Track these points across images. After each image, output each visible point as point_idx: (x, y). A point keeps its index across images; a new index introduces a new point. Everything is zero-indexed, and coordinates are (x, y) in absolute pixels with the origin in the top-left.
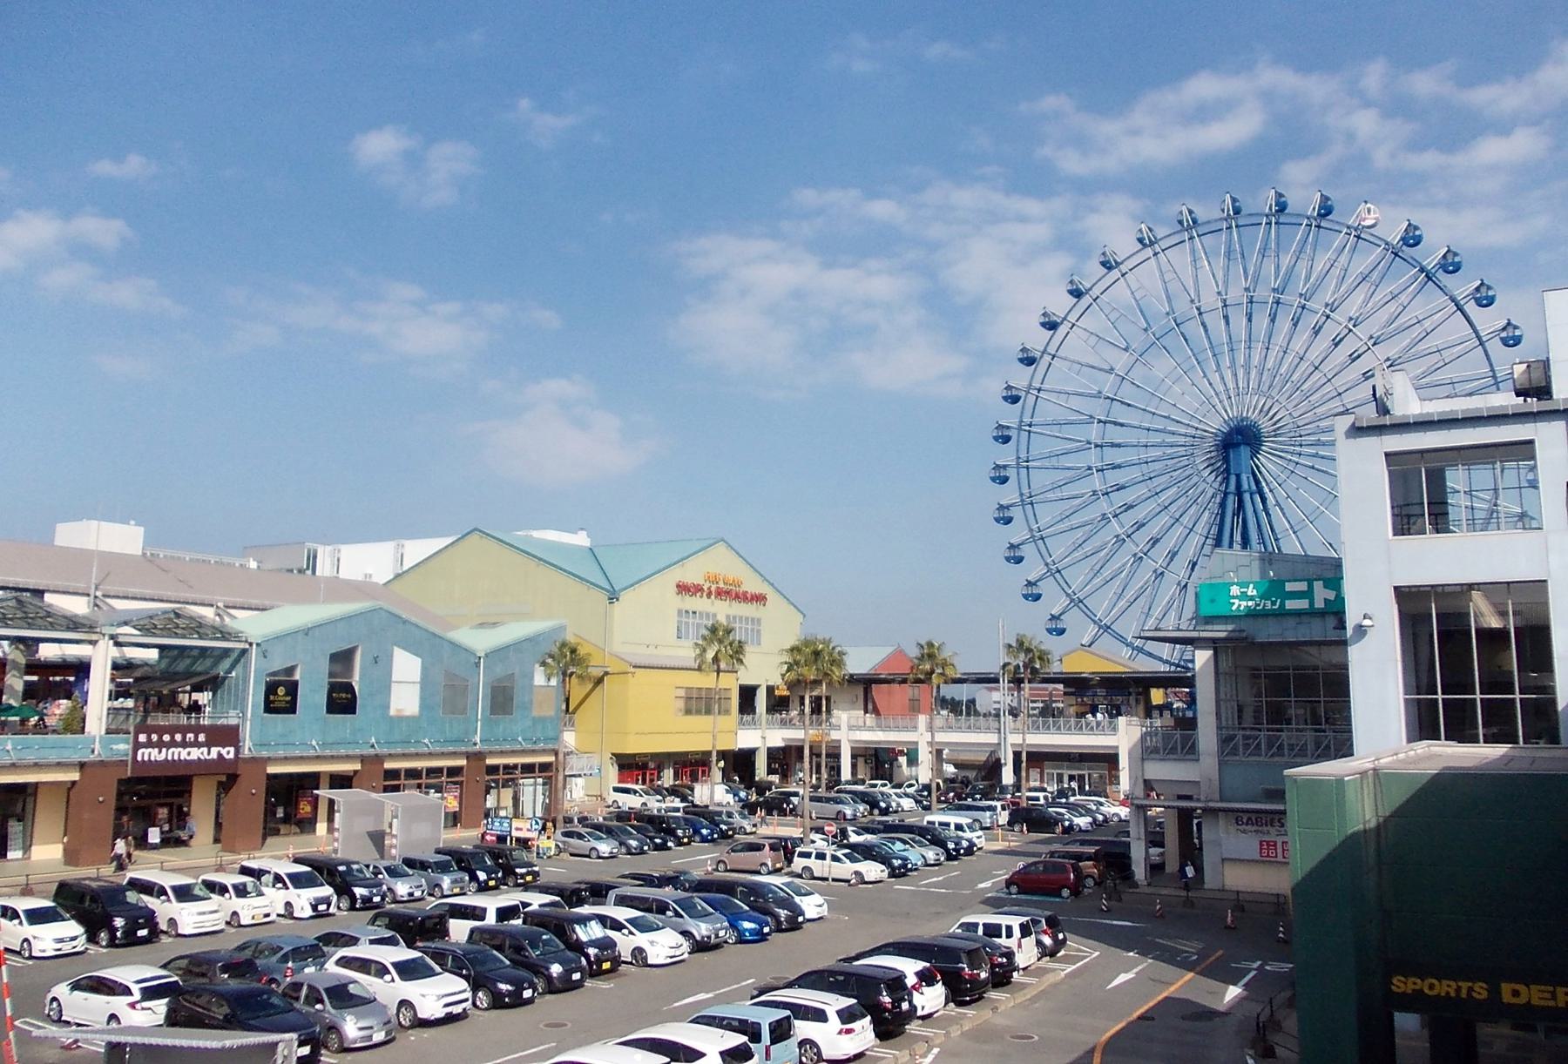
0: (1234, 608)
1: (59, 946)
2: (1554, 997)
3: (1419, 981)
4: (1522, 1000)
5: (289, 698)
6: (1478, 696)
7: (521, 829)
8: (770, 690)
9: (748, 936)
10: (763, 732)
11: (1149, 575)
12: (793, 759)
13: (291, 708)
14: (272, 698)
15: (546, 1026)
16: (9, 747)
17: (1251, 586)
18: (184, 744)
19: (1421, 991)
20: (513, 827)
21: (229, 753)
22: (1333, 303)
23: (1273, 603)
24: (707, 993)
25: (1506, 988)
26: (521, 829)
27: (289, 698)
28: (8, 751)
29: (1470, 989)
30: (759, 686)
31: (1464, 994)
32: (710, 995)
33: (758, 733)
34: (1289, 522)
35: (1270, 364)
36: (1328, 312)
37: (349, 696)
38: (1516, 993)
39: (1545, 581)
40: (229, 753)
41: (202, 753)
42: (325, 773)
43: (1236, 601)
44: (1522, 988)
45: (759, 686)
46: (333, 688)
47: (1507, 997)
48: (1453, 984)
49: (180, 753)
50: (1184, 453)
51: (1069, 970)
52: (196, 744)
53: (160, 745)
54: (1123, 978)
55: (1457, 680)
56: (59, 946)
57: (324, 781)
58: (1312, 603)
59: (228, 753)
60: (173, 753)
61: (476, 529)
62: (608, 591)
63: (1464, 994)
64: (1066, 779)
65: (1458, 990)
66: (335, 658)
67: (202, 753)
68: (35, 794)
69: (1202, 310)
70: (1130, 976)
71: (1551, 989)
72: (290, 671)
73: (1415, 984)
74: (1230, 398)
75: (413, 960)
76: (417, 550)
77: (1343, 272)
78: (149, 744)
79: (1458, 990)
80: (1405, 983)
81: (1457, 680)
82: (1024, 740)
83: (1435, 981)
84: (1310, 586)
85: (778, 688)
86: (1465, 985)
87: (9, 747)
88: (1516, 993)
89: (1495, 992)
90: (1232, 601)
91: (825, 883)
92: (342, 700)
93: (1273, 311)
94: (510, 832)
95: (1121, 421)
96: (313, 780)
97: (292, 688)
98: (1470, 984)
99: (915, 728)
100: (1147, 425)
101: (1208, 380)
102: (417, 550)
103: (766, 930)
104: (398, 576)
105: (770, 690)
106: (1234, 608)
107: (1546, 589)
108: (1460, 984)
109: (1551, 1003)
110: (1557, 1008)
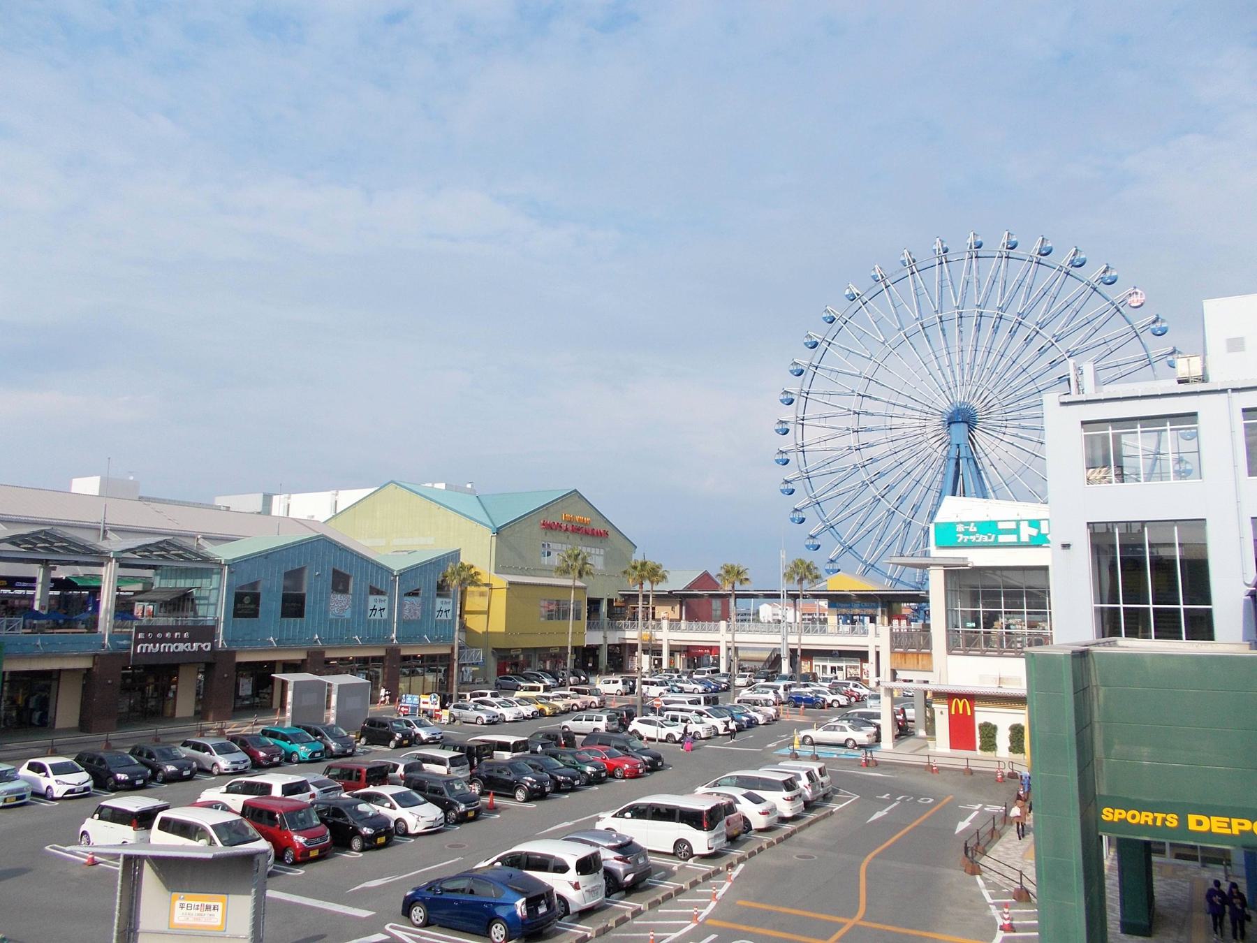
0: (959, 541)
1: (235, 766)
2: (1230, 826)
3: (1123, 812)
4: (1204, 828)
5: (252, 606)
6: (1151, 606)
7: (427, 703)
8: (610, 601)
9: (563, 786)
10: (605, 634)
11: (884, 513)
12: (627, 654)
13: (254, 614)
14: (239, 606)
15: (450, 846)
16: (39, 643)
17: (972, 524)
18: (173, 640)
19: (1126, 819)
20: (422, 701)
21: (206, 646)
22: (1023, 312)
23: (989, 537)
24: (569, 821)
25: (1192, 819)
26: (427, 703)
27: (252, 606)
28: (38, 646)
29: (1164, 820)
30: (603, 599)
31: (1159, 823)
32: (571, 823)
33: (601, 634)
34: (1002, 478)
35: (978, 361)
36: (1020, 319)
37: (300, 605)
38: (1199, 823)
39: (1204, 520)
40: (206, 646)
41: (187, 647)
42: (280, 661)
43: (961, 536)
44: (1203, 818)
45: (603, 599)
46: (286, 598)
47: (1192, 826)
48: (1150, 814)
49: (170, 647)
50: (918, 425)
51: (838, 808)
52: (182, 640)
53: (154, 641)
54: (878, 815)
55: (1135, 594)
56: (235, 766)
57: (279, 667)
58: (1019, 538)
59: (206, 647)
60: (165, 647)
61: (392, 482)
62: (491, 528)
63: (1159, 823)
64: (829, 670)
65: (1155, 820)
66: (288, 575)
67: (187, 647)
68: (58, 679)
69: (943, 319)
70: (884, 813)
71: (1227, 820)
72: (254, 585)
73: (1120, 814)
74: (956, 386)
75: (404, 793)
76: (348, 497)
77: (1029, 290)
78: (146, 640)
79: (1155, 820)
80: (1113, 814)
81: (1135, 594)
82: (800, 640)
83: (1136, 813)
84: (1018, 525)
85: (616, 601)
86: (1160, 816)
87: (39, 643)
88: (1199, 823)
89: (1183, 821)
90: (958, 535)
91: (653, 743)
92: (294, 606)
93: (978, 322)
94: (419, 705)
95: (876, 397)
96: (272, 666)
97: (256, 598)
98: (1164, 815)
99: (717, 630)
100: (894, 402)
101: (942, 372)
102: (348, 497)
103: (577, 783)
104: (333, 516)
105: (610, 601)
106: (959, 541)
107: (1205, 524)
108: (1156, 814)
109: (1228, 831)
110: (1232, 835)
